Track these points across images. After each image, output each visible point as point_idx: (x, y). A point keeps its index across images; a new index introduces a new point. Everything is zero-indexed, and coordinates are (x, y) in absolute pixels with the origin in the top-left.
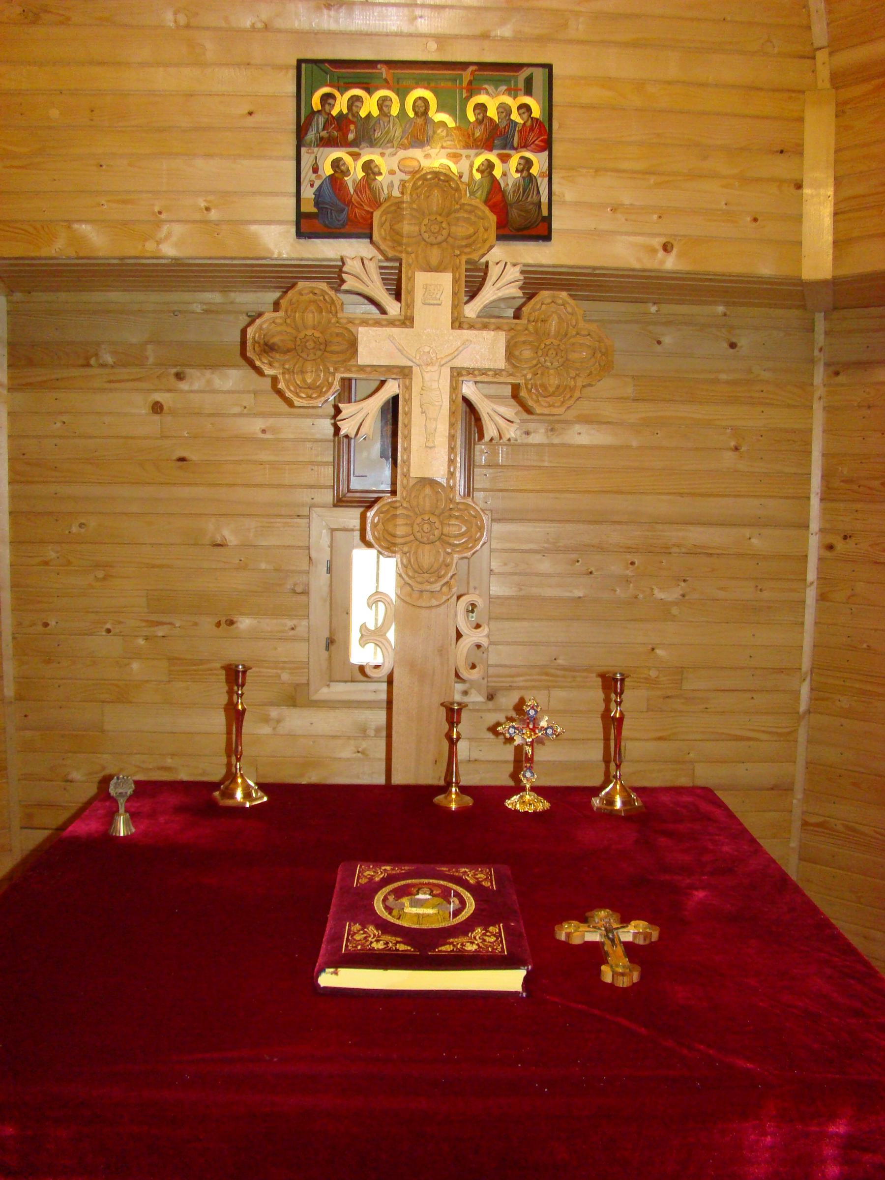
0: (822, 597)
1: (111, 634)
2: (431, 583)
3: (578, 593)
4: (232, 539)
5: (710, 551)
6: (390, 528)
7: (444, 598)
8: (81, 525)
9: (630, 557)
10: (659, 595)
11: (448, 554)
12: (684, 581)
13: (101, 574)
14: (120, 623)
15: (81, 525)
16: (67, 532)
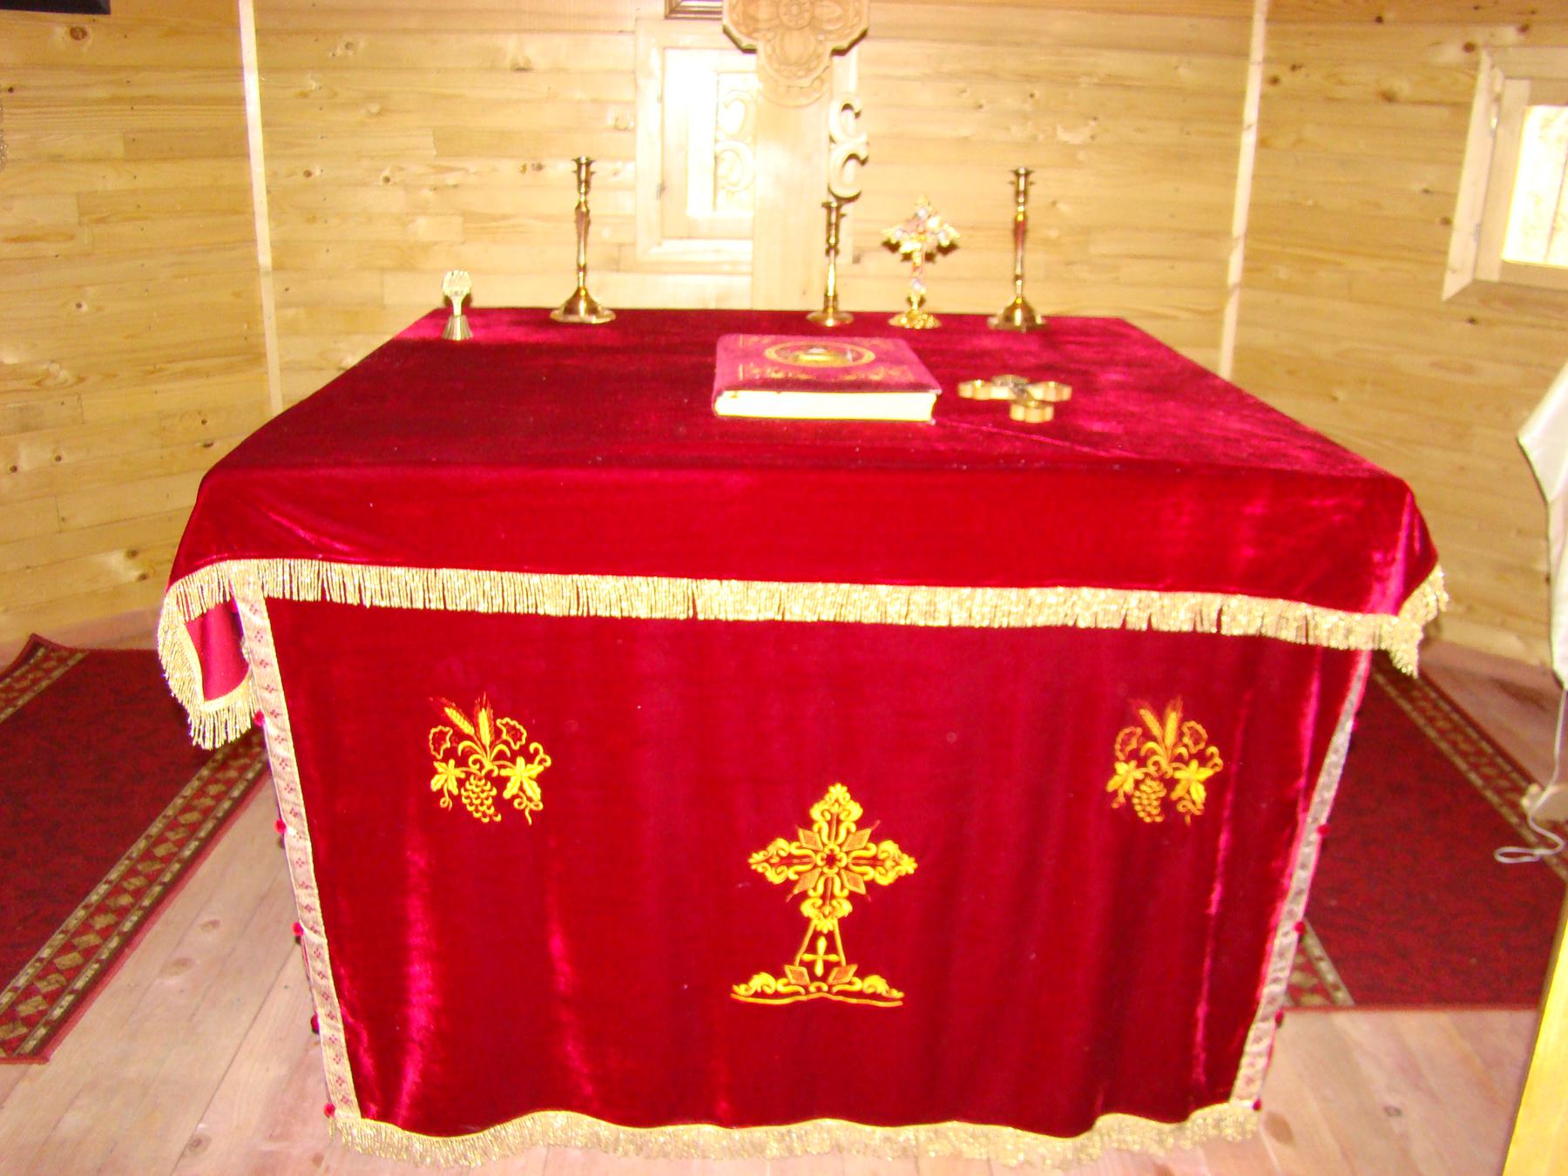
0: (1262, 143)
1: (390, 183)
2: (799, 77)
3: (964, 132)
4: (540, 63)
5: (1128, 83)
6: (751, 10)
7: (816, 96)
8: (348, 46)
9: (1028, 87)
10: (1063, 136)
11: (821, 42)
12: (1095, 119)
13: (375, 108)
14: (401, 169)
15: (348, 46)
16: (331, 54)
